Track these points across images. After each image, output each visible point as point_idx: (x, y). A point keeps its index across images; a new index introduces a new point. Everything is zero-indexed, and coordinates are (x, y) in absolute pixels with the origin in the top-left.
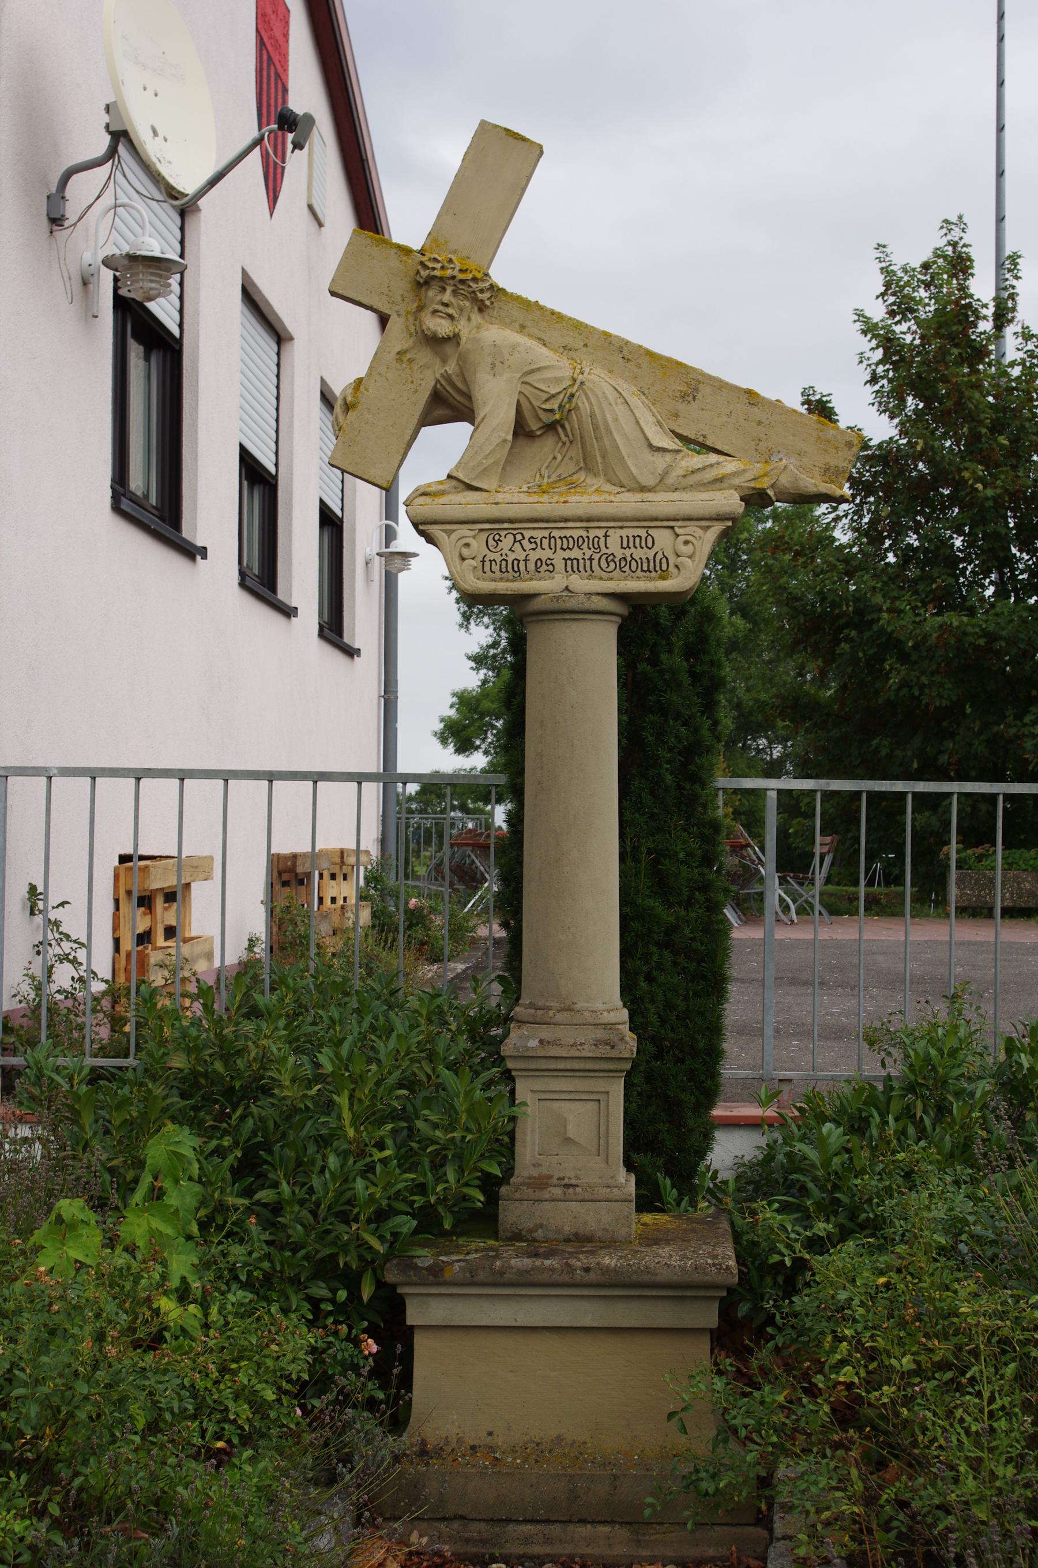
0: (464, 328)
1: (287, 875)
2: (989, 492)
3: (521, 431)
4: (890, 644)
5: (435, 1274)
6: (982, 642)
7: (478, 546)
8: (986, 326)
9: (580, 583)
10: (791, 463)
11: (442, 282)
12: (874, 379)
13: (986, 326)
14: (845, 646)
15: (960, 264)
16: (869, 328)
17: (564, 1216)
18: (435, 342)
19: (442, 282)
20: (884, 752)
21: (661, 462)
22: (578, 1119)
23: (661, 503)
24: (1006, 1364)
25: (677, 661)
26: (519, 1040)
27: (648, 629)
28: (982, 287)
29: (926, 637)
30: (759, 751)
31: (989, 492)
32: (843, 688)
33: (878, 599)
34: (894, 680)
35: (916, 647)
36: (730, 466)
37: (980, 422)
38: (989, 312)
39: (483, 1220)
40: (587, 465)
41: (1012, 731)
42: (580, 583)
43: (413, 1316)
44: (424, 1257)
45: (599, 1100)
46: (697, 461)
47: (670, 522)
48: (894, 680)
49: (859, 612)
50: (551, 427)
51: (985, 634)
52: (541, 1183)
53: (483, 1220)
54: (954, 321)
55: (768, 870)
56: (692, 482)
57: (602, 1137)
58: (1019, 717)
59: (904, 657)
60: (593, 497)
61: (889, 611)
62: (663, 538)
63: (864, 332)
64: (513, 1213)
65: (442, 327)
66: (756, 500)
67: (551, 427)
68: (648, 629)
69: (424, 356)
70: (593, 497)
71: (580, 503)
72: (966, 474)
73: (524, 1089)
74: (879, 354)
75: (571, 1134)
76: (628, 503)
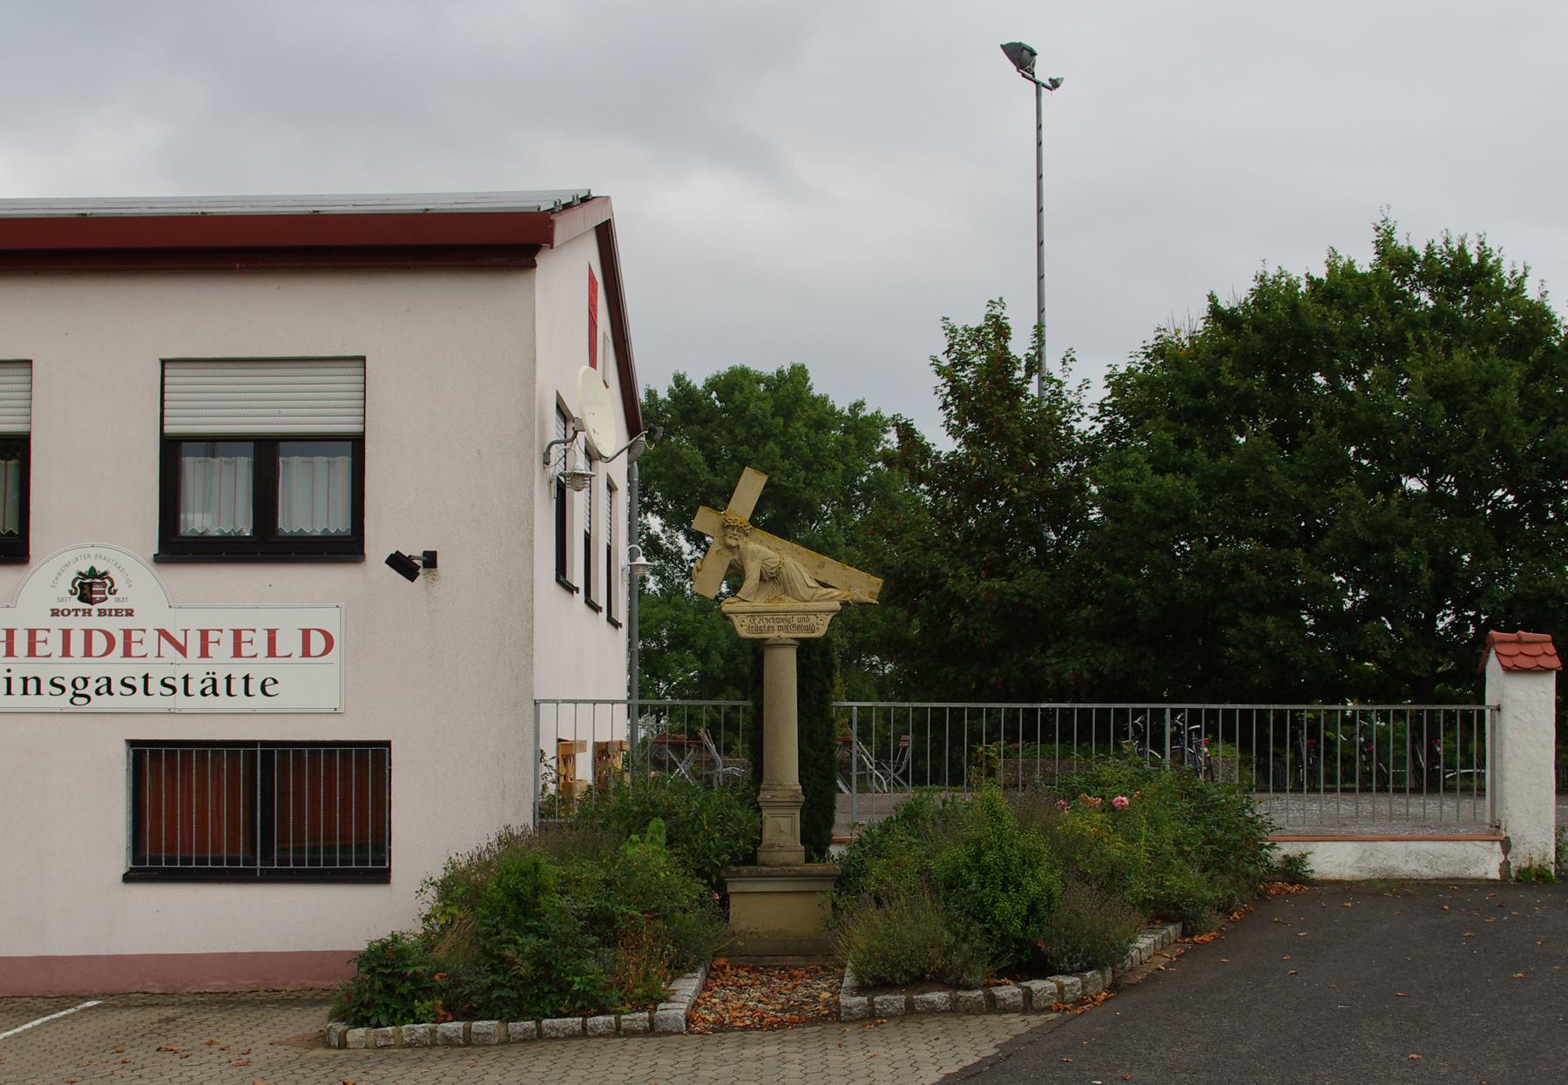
0: (741, 543)
1: (602, 751)
2: (1022, 494)
3: (762, 579)
4: (955, 600)
5: (738, 875)
6: (1016, 599)
7: (747, 621)
8: (1020, 374)
9: (783, 635)
10: (857, 591)
11: (733, 527)
12: (945, 406)
13: (1020, 374)
14: (923, 601)
15: (1001, 330)
16: (940, 371)
17: (781, 857)
18: (730, 548)
19: (733, 527)
20: (951, 677)
21: (812, 592)
22: (784, 823)
23: (812, 606)
24: (701, 442)
25: (818, 658)
26: (764, 796)
27: (806, 649)
28: (1019, 347)
29: (978, 595)
30: (872, 667)
31: (1022, 494)
32: (924, 630)
33: (946, 569)
34: (956, 625)
35: (973, 601)
36: (836, 592)
37: (1016, 444)
38: (1023, 363)
39: (751, 859)
40: (786, 592)
41: (1039, 661)
42: (783, 635)
43: (730, 889)
44: (733, 868)
45: (791, 816)
46: (825, 591)
47: (815, 612)
48: (956, 625)
49: (934, 577)
50: (773, 579)
51: (1020, 594)
52: (772, 846)
53: (751, 859)
54: (1000, 364)
55: (855, 739)
56: (821, 599)
57: (793, 831)
58: (1043, 651)
59: (965, 609)
60: (788, 604)
61: (954, 577)
62: (812, 618)
63: (938, 373)
64: (761, 856)
65: (734, 543)
66: (845, 604)
67: (773, 579)
68: (806, 649)
69: (727, 552)
70: (788, 604)
71: (783, 606)
72: (1007, 481)
73: (765, 813)
74: (947, 390)
75: (782, 830)
76: (800, 606)
